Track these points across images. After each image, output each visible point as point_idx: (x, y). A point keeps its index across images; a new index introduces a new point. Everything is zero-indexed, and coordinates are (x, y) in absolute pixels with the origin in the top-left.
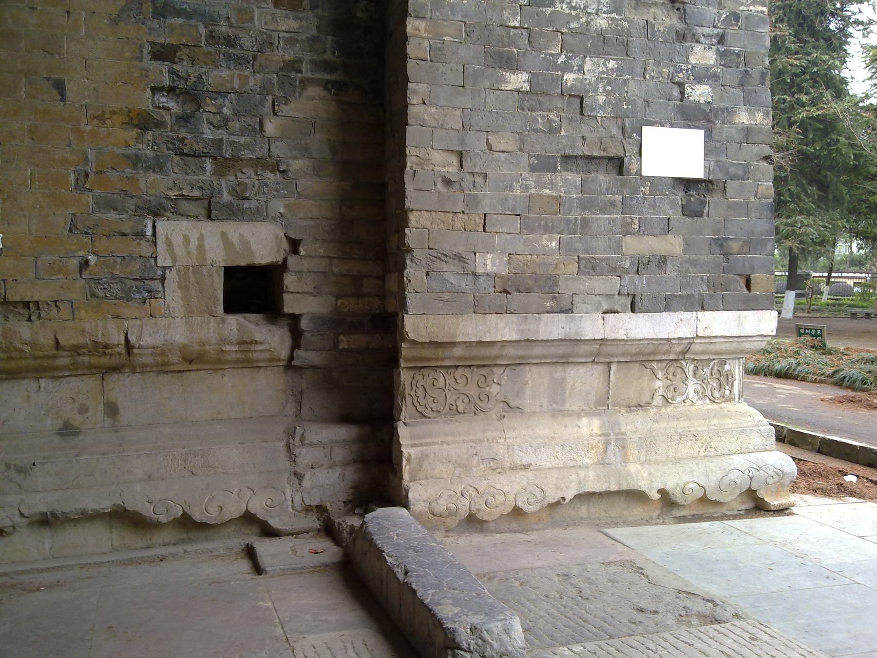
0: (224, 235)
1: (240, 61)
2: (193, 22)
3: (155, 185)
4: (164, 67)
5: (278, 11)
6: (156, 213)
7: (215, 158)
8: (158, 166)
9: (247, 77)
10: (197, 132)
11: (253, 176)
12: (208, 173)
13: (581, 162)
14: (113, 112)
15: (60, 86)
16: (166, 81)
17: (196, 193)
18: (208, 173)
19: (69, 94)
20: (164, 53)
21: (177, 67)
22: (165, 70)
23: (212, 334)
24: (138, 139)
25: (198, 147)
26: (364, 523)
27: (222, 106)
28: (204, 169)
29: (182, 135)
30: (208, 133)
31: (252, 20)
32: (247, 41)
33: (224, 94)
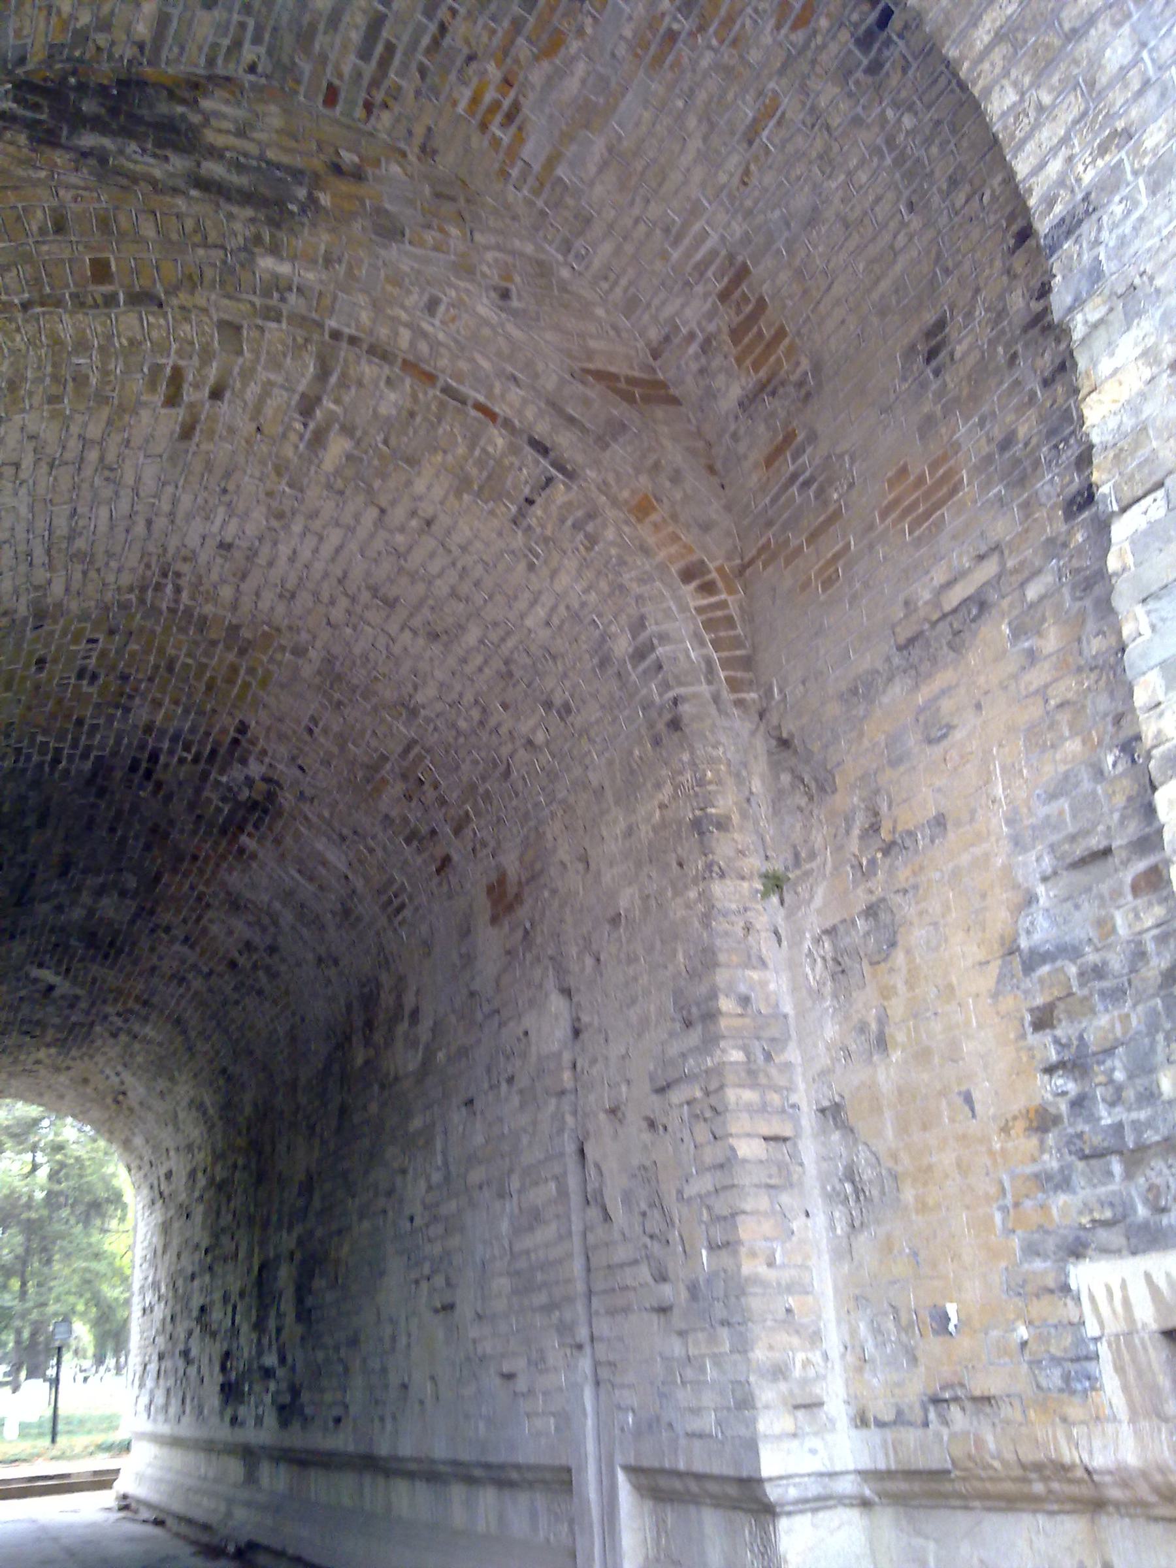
0: (1148, 1277)
1: (1115, 995)
2: (1059, 963)
3: (1064, 1209)
4: (1046, 1037)
5: (1139, 901)
6: (1077, 1250)
7: (1120, 1153)
8: (1062, 1182)
9: (1128, 1016)
10: (1093, 1119)
11: (1166, 1171)
12: (1118, 1178)
13: (309, 1301)
14: (1015, 1118)
15: (968, 1099)
16: (1053, 1056)
17: (1108, 1214)
18: (1118, 1178)
19: (977, 1107)
20: (1043, 1020)
21: (1059, 1032)
22: (1048, 1039)
23: (1167, 1454)
24: (1042, 1148)
25: (1097, 1140)
26: (50, 1218)
27: (1113, 1069)
28: (1110, 1174)
29: (1079, 1128)
30: (1107, 1119)
31: (1114, 930)
32: (1117, 962)
33: (1109, 1051)
